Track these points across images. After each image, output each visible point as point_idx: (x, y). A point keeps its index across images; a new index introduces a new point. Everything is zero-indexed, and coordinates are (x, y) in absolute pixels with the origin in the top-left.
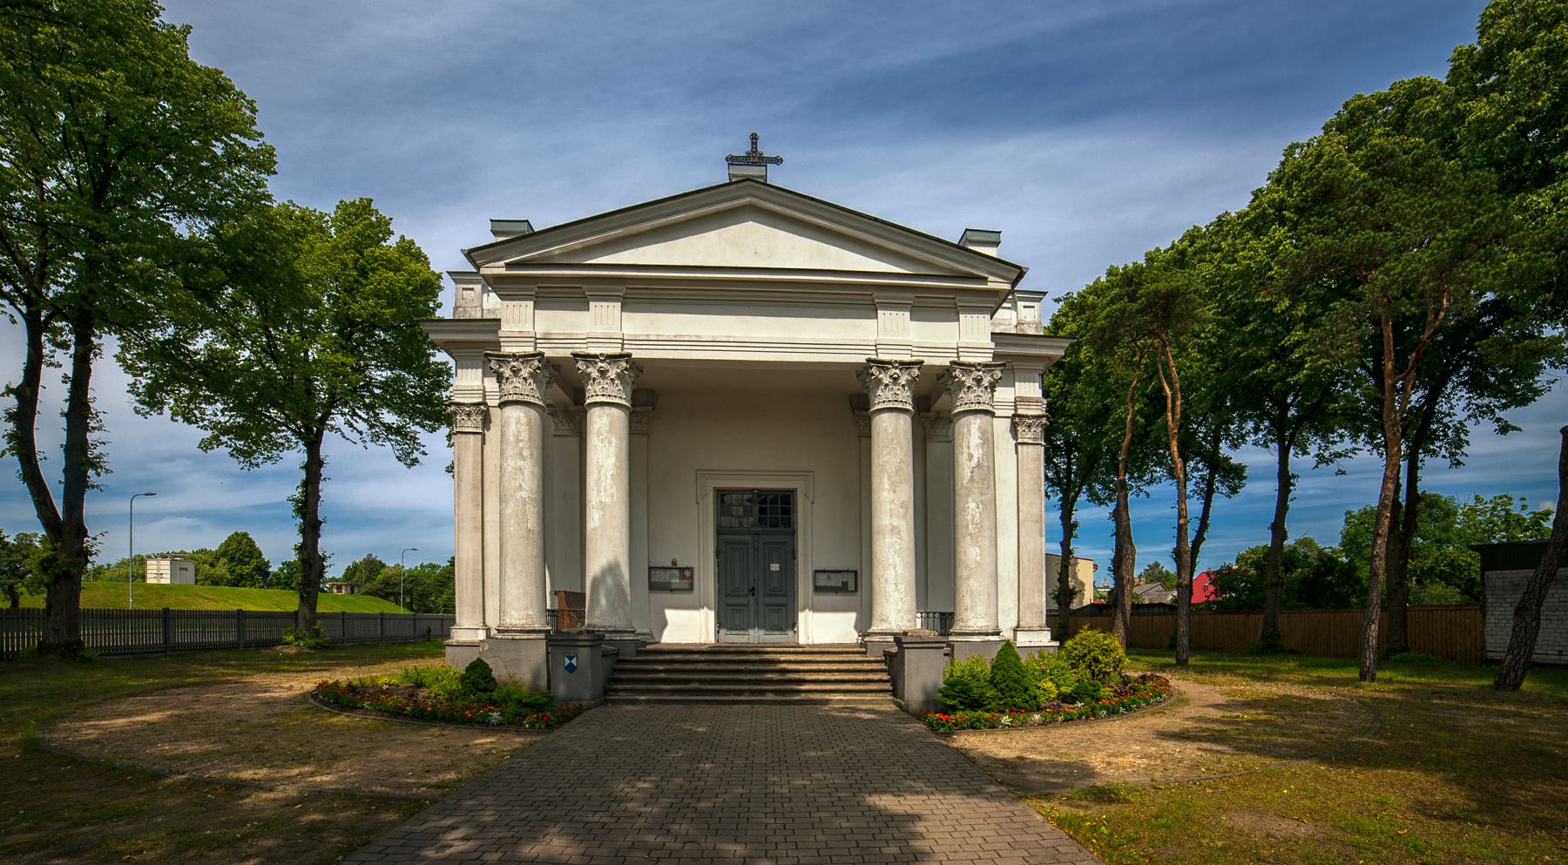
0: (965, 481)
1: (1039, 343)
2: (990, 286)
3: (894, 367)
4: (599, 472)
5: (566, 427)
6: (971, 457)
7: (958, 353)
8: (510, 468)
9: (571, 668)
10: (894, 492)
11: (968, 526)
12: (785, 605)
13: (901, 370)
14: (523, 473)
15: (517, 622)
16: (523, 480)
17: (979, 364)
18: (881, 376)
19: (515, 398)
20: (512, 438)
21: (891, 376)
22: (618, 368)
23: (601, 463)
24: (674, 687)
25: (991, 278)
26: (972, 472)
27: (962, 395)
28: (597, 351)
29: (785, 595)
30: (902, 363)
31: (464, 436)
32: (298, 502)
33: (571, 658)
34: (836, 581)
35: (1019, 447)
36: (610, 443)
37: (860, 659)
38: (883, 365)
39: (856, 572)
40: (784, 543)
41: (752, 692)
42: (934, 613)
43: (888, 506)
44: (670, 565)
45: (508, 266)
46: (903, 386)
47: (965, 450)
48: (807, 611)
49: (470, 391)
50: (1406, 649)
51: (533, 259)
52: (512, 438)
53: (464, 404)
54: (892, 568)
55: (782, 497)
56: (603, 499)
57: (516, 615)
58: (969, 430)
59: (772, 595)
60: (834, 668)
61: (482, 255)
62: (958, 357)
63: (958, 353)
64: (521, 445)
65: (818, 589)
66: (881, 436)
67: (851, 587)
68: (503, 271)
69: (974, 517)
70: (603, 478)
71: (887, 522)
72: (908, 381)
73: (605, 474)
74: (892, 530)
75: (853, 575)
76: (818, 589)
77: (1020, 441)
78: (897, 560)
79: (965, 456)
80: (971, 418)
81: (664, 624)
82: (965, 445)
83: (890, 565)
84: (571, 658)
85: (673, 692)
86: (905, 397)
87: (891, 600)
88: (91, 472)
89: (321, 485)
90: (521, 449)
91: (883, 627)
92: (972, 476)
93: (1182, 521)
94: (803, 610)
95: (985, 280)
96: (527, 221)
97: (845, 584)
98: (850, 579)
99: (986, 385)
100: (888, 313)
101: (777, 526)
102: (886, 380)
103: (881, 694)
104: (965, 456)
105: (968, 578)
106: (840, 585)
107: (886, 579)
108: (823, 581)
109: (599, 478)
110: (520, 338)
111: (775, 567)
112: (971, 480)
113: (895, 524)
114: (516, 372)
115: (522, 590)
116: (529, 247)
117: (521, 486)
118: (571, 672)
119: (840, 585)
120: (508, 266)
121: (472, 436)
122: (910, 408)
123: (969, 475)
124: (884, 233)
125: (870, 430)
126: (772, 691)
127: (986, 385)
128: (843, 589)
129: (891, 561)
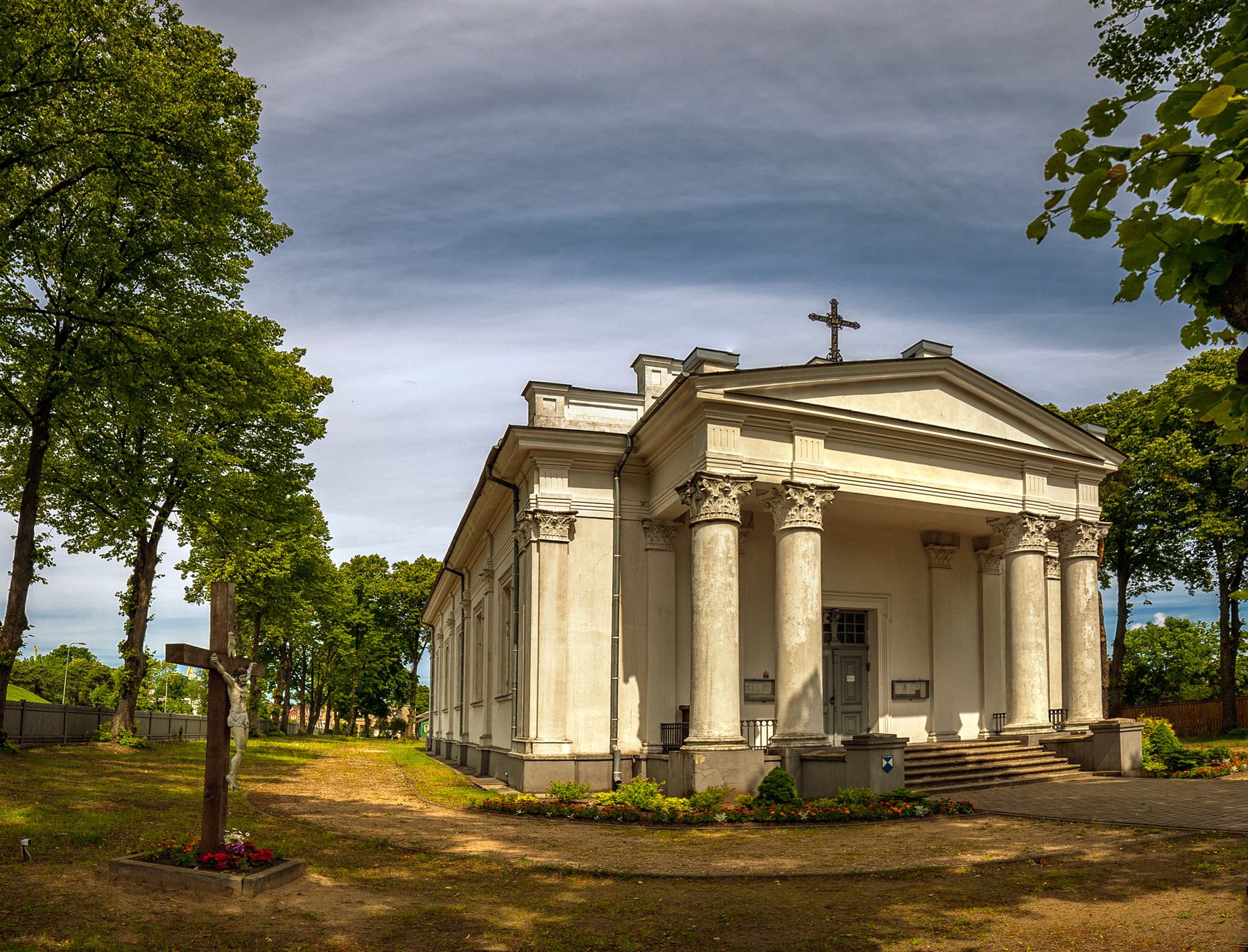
0: (1081, 610)
1: (606, 441)
2: (1105, 466)
3: (810, 490)
4: (806, 591)
5: (661, 541)
6: (1086, 591)
7: (791, 473)
8: (719, 584)
9: (888, 769)
10: (1039, 616)
11: (1085, 643)
12: (859, 712)
13: (732, 484)
14: (732, 589)
15: (727, 734)
16: (732, 596)
17: (813, 485)
18: (710, 489)
19: (725, 517)
20: (721, 555)
21: (1036, 526)
22: (823, 497)
23: (807, 583)
24: (943, 778)
25: (1107, 461)
26: (1088, 603)
27: (707, 503)
28: (808, 482)
29: (860, 703)
30: (1046, 517)
31: (547, 544)
32: (125, 598)
33: (887, 760)
34: (910, 690)
35: (1048, 581)
36: (815, 565)
37: (1018, 749)
38: (799, 487)
39: (927, 682)
40: (860, 658)
41: (985, 778)
42: (748, 722)
43: (1033, 627)
44: (762, 678)
45: (727, 394)
46: (734, 499)
47: (1082, 586)
48: (887, 716)
49: (558, 500)
50: (1235, 727)
51: (762, 390)
52: (721, 555)
53: (551, 513)
54: (1037, 675)
55: (857, 615)
56: (810, 616)
57: (726, 727)
58: (1085, 571)
59: (848, 704)
60: (1020, 755)
61: (702, 380)
62: (792, 477)
63: (791, 473)
64: (730, 562)
65: (895, 697)
66: (1026, 572)
67: (923, 694)
68: (721, 398)
69: (1090, 636)
70: (809, 597)
71: (1033, 640)
72: (738, 495)
73: (812, 594)
74: (1037, 646)
75: (924, 685)
76: (895, 697)
77: (1049, 576)
78: (1041, 669)
79: (1082, 590)
80: (1086, 562)
81: (960, 725)
82: (1081, 582)
83: (1036, 673)
84: (887, 760)
85: (976, 779)
86: (733, 510)
87: (1038, 701)
88: (36, 565)
89: (155, 582)
90: (731, 566)
91: (1082, 719)
92: (1087, 606)
93: (1103, 639)
94: (884, 715)
95: (1102, 461)
96: (697, 348)
97: (918, 692)
98: (923, 688)
99: (818, 505)
100: (804, 439)
101: (853, 642)
102: (1033, 529)
103: (1072, 771)
104: (1082, 590)
105: (1085, 682)
106: (914, 693)
107: (1033, 686)
108: (899, 690)
109: (806, 597)
110: (721, 461)
111: (851, 679)
112: (1087, 608)
113: (1040, 641)
114: (726, 492)
115: (731, 703)
116: (750, 380)
117: (730, 601)
118: (887, 772)
119: (914, 693)
120: (727, 394)
121: (557, 545)
122: (738, 520)
123: (1086, 605)
124: (1040, 417)
125: (740, 547)
126: (999, 776)
127: (818, 505)
128: (916, 696)
129: (1037, 670)
